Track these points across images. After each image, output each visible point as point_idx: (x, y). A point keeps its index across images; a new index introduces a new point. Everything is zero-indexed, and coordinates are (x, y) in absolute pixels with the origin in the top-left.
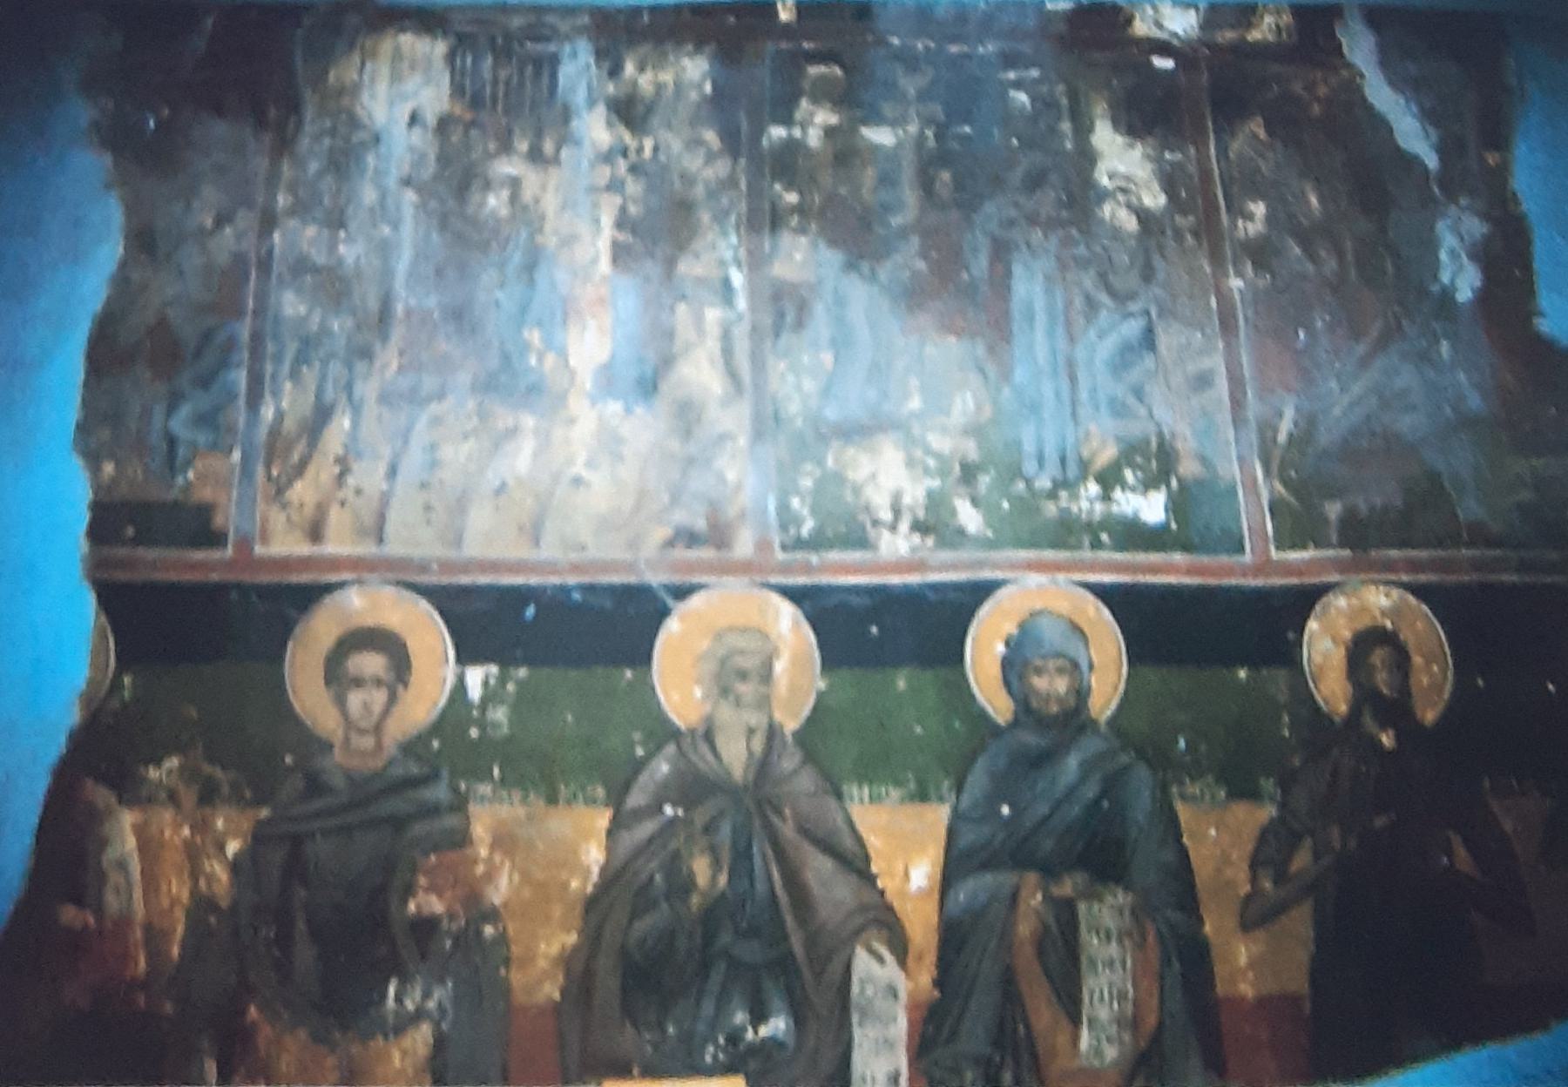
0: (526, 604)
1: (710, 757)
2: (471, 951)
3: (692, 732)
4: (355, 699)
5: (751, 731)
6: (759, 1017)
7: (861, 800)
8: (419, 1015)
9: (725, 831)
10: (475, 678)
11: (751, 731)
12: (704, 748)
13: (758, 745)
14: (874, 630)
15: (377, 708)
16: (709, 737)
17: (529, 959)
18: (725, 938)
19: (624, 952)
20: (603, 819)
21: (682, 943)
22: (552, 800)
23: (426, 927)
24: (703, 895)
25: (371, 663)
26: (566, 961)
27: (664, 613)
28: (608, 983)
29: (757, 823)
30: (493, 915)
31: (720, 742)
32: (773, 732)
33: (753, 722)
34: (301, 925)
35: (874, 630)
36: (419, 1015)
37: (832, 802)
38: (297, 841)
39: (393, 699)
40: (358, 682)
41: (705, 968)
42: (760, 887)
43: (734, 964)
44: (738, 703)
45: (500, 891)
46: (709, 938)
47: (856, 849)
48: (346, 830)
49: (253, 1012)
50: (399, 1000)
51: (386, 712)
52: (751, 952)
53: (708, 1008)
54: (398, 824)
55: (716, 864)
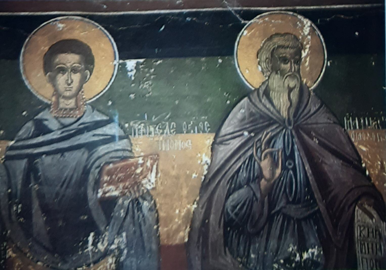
0: (85, 214)
1: (269, 105)
2: (136, 211)
3: (257, 90)
4: (61, 79)
5: (290, 90)
6: (302, 248)
7: (355, 127)
8: (106, 254)
9: (279, 144)
10: (131, 64)
11: (290, 90)
12: (264, 100)
13: (294, 96)
14: (357, 34)
15: (75, 85)
16: (267, 93)
17: (170, 219)
18: (282, 203)
19: (224, 212)
20: (209, 139)
21: (256, 207)
22: (179, 131)
23: (108, 204)
24: (268, 180)
25: (71, 59)
26: (191, 220)
27: (240, 27)
28: (216, 232)
29: (296, 140)
30: (146, 196)
31: (273, 95)
32: (302, 89)
33: (292, 84)
34: (36, 205)
35: (357, 34)
36: (106, 254)
37: (338, 128)
38: (32, 158)
39: (84, 80)
40: (63, 70)
41: (270, 219)
42: (300, 175)
43: (287, 218)
44: (282, 74)
45: (150, 182)
46: (272, 205)
47: (355, 156)
48: (62, 151)
49: (10, 253)
50: (95, 244)
51: (80, 88)
52: (294, 211)
53: (273, 243)
54: (91, 147)
55: (274, 164)
